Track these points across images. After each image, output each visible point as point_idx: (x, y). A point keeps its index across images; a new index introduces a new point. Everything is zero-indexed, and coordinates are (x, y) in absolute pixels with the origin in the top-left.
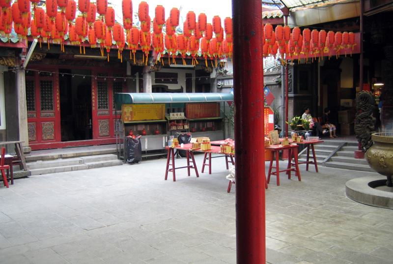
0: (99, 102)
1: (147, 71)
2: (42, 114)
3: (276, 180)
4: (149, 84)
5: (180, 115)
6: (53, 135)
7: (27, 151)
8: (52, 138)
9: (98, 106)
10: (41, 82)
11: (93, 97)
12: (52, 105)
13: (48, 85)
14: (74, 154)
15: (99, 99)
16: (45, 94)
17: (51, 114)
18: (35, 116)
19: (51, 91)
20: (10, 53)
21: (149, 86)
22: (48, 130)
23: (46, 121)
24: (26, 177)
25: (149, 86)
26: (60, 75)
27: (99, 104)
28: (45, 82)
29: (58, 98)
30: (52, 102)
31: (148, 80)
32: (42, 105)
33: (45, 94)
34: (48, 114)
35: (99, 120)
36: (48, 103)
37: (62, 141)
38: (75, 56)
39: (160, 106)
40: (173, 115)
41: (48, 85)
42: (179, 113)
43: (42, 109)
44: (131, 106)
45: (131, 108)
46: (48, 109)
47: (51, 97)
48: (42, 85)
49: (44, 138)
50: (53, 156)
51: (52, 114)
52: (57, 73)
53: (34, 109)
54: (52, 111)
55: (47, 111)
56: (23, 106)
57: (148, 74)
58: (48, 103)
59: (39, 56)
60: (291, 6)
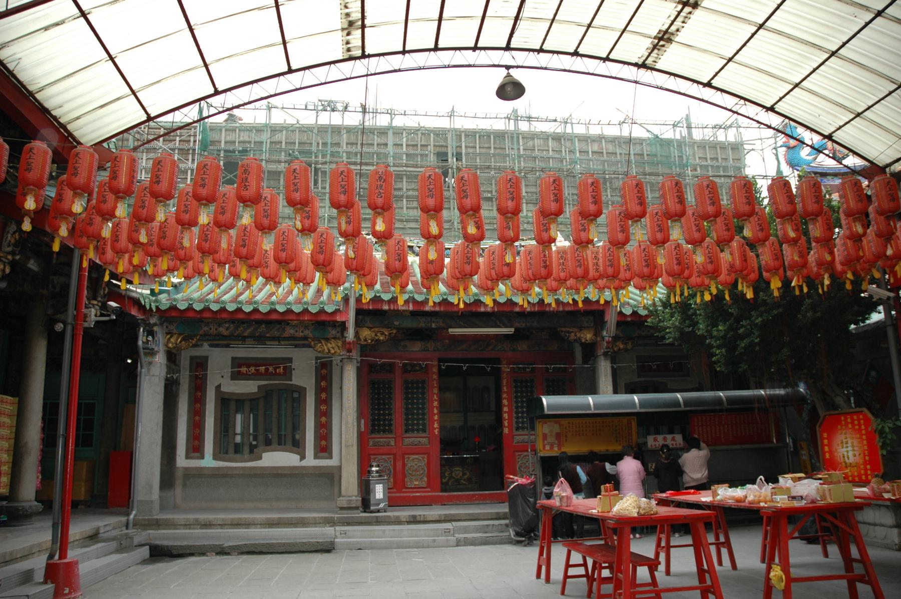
0: (517, 418)
1: (600, 352)
2: (406, 441)
3: (671, 559)
4: (606, 376)
5: (673, 439)
6: (426, 479)
7: (354, 505)
8: (424, 484)
9: (515, 425)
10: (406, 382)
11: (506, 409)
12: (424, 425)
13: (417, 388)
14: (440, 515)
15: (517, 413)
16: (412, 404)
17: (421, 440)
18: (393, 443)
19: (424, 398)
20: (334, 332)
21: (605, 380)
22: (416, 470)
23: (413, 454)
24: (328, 551)
25: (605, 380)
26: (440, 366)
27: (517, 423)
28: (412, 382)
29: (435, 411)
30: (424, 419)
31: (603, 368)
32: (406, 425)
33: (412, 404)
34: (416, 440)
35: (517, 454)
36: (418, 420)
37: (443, 491)
38: (450, 330)
39: (625, 420)
40: (655, 440)
41: (417, 388)
42: (669, 437)
43: (406, 431)
44: (556, 423)
45: (557, 426)
46: (418, 430)
47: (423, 408)
48: (407, 388)
49: (409, 485)
50: (398, 517)
51: (425, 441)
52: (435, 363)
53: (390, 431)
54: (423, 435)
55: (416, 434)
56: (351, 422)
57: (602, 358)
58: (418, 420)
59: (382, 334)
60: (889, 161)
